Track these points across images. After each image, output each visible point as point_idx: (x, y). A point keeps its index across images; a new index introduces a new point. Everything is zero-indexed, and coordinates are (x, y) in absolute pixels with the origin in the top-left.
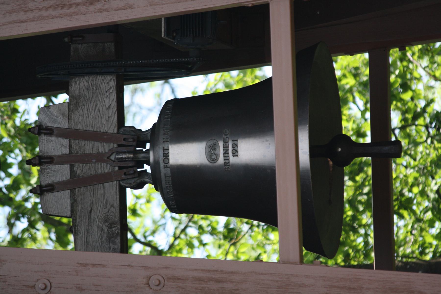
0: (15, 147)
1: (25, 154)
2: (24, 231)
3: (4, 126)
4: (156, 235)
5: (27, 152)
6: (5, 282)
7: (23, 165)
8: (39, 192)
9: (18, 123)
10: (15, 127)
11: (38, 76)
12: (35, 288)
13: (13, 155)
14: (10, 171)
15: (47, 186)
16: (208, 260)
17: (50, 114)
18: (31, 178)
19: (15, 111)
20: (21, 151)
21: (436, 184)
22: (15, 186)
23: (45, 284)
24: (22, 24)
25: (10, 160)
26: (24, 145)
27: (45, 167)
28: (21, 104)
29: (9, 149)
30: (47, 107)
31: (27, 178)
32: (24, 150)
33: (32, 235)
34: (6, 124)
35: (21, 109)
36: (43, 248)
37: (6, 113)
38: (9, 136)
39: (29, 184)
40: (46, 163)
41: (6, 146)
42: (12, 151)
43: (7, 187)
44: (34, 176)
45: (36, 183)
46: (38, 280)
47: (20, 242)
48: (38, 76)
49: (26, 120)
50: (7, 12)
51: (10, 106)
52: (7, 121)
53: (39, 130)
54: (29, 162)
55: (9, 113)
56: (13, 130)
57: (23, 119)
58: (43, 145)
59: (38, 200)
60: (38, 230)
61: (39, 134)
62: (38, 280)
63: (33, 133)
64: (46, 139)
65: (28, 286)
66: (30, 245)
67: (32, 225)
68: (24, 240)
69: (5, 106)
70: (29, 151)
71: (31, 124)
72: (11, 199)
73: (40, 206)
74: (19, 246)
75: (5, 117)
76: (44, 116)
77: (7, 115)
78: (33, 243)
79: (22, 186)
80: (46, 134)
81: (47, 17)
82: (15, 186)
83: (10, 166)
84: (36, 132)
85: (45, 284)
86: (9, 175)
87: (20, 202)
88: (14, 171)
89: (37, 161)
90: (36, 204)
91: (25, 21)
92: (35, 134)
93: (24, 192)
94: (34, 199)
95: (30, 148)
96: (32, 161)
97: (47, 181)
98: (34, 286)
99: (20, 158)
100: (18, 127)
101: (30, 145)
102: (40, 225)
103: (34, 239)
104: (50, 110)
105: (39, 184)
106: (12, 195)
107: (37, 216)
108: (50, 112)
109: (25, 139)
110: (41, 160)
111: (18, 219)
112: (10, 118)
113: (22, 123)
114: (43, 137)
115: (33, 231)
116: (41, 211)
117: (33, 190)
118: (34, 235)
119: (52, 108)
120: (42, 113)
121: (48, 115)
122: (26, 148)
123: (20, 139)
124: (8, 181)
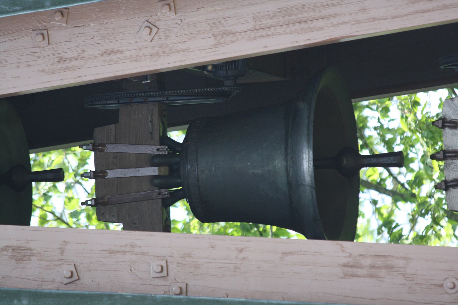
0: (417, 140)
1: (426, 148)
2: (427, 228)
3: (404, 120)
4: (366, 222)
5: (428, 147)
6: (412, 280)
7: (426, 159)
8: (444, 187)
9: (419, 117)
10: (416, 120)
11: (442, 67)
12: (443, 287)
13: (414, 150)
14: (412, 165)
15: (452, 181)
16: (443, 248)
17: (454, 107)
18: (433, 173)
19: (416, 103)
20: (422, 145)
21: (158, 150)
22: (418, 182)
23: (453, 283)
24: (425, 14)
25: (411, 155)
26: (425, 140)
27: (449, 161)
28: (421, 96)
29: (411, 144)
30: (450, 99)
31: (429, 173)
32: (425, 145)
33: (436, 232)
34: (407, 118)
35: (422, 102)
36: (446, 245)
37: (407, 106)
38: (410, 129)
39: (432, 180)
40: (451, 157)
41: (407, 140)
42: (413, 146)
43: (409, 183)
44: (436, 172)
45: (438, 178)
46: (446, 279)
47: (424, 240)
48: (442, 67)
49: (427, 113)
50: (410, 2)
51: (411, 99)
52: (408, 115)
53: (444, 123)
54: (433, 157)
55: (410, 107)
56: (413, 124)
57: (424, 113)
58: (448, 139)
59: (443, 196)
60: (442, 227)
61: (443, 127)
62: (446, 279)
63: (437, 126)
64: (450, 133)
65: (436, 285)
66: (434, 242)
67: (436, 221)
68: (429, 238)
69: (406, 99)
70: (430, 146)
71: (433, 118)
72: (414, 195)
73: (444, 202)
74: (424, 243)
75: (406, 111)
76: (448, 109)
77: (408, 108)
78: (437, 239)
79: (424, 182)
80: (450, 127)
81: (451, 5)
82: (418, 182)
83: (412, 161)
84: (440, 125)
85: (453, 283)
86: (412, 171)
87: (424, 198)
88: (416, 166)
89: (441, 155)
90: (440, 199)
91: (428, 11)
92: (440, 128)
93: (427, 187)
94: (438, 195)
95: (431, 142)
96: (437, 155)
97: (451, 176)
98: (441, 286)
99: (421, 153)
100: (420, 121)
101: (432, 138)
102: (444, 222)
103: (439, 236)
104: (454, 102)
105: (443, 179)
106: (414, 191)
107: (442, 212)
108: (454, 104)
109: (426, 133)
110: (444, 155)
111: (423, 215)
112: (410, 111)
113: (424, 116)
114: (447, 130)
115: (438, 228)
116: (445, 207)
117: (438, 186)
118: (438, 232)
119: (456, 100)
120: (446, 105)
121: (453, 107)
122: (427, 143)
123: (421, 133)
124: (411, 177)
